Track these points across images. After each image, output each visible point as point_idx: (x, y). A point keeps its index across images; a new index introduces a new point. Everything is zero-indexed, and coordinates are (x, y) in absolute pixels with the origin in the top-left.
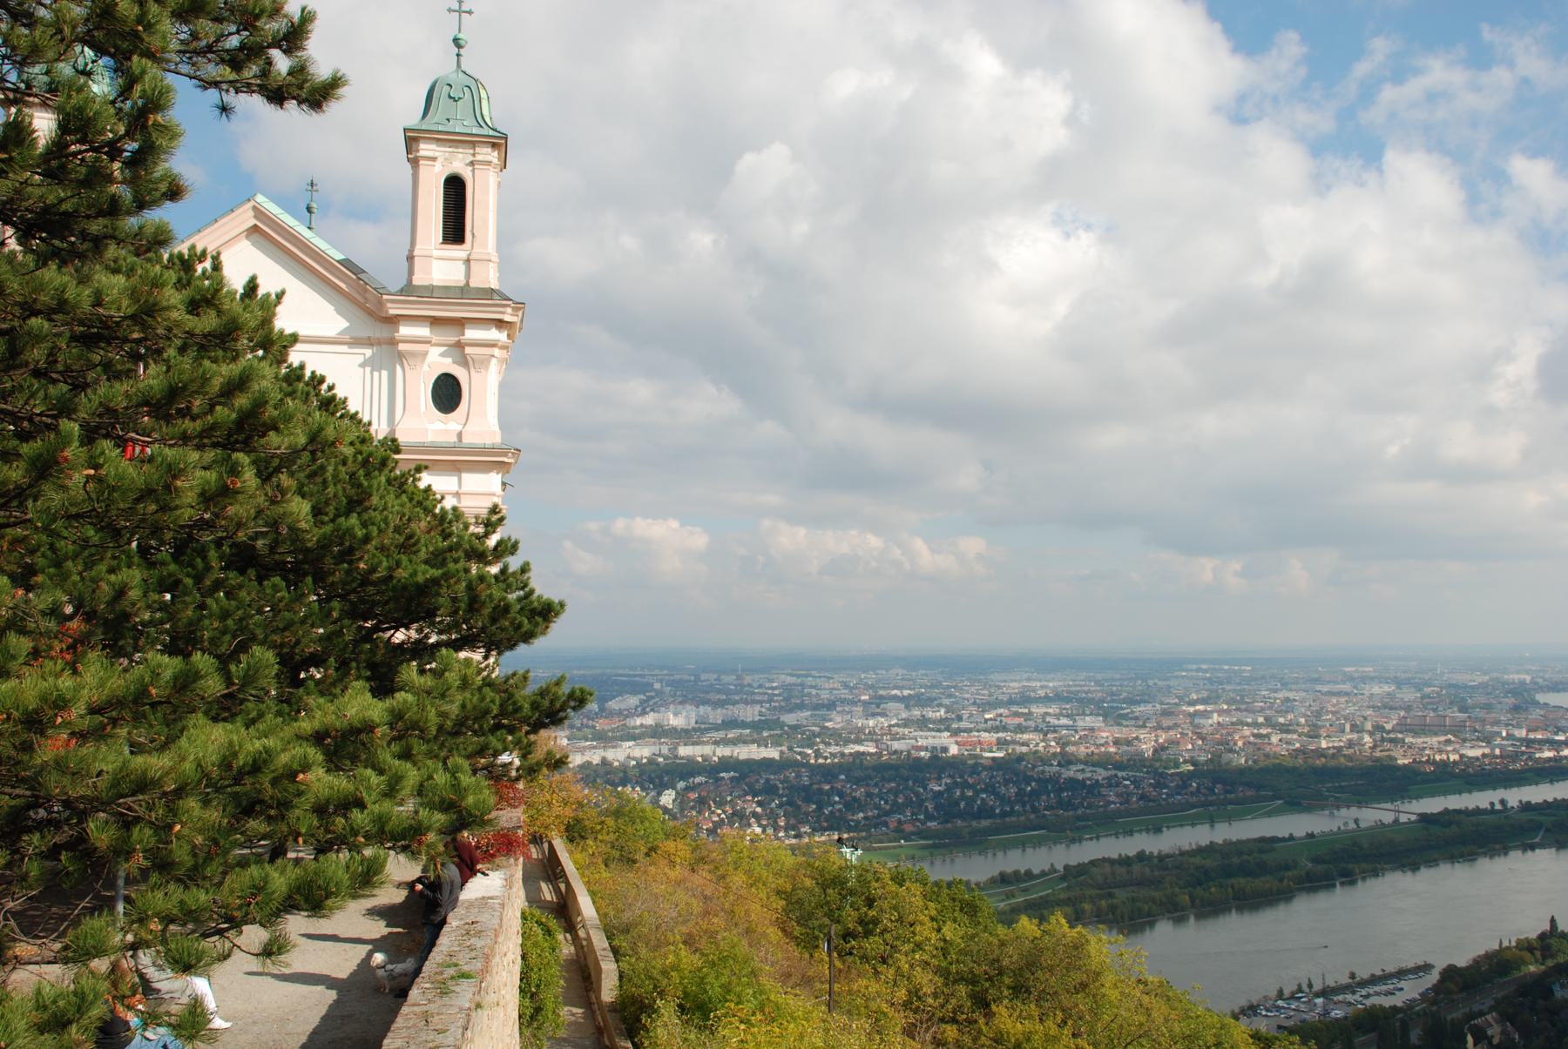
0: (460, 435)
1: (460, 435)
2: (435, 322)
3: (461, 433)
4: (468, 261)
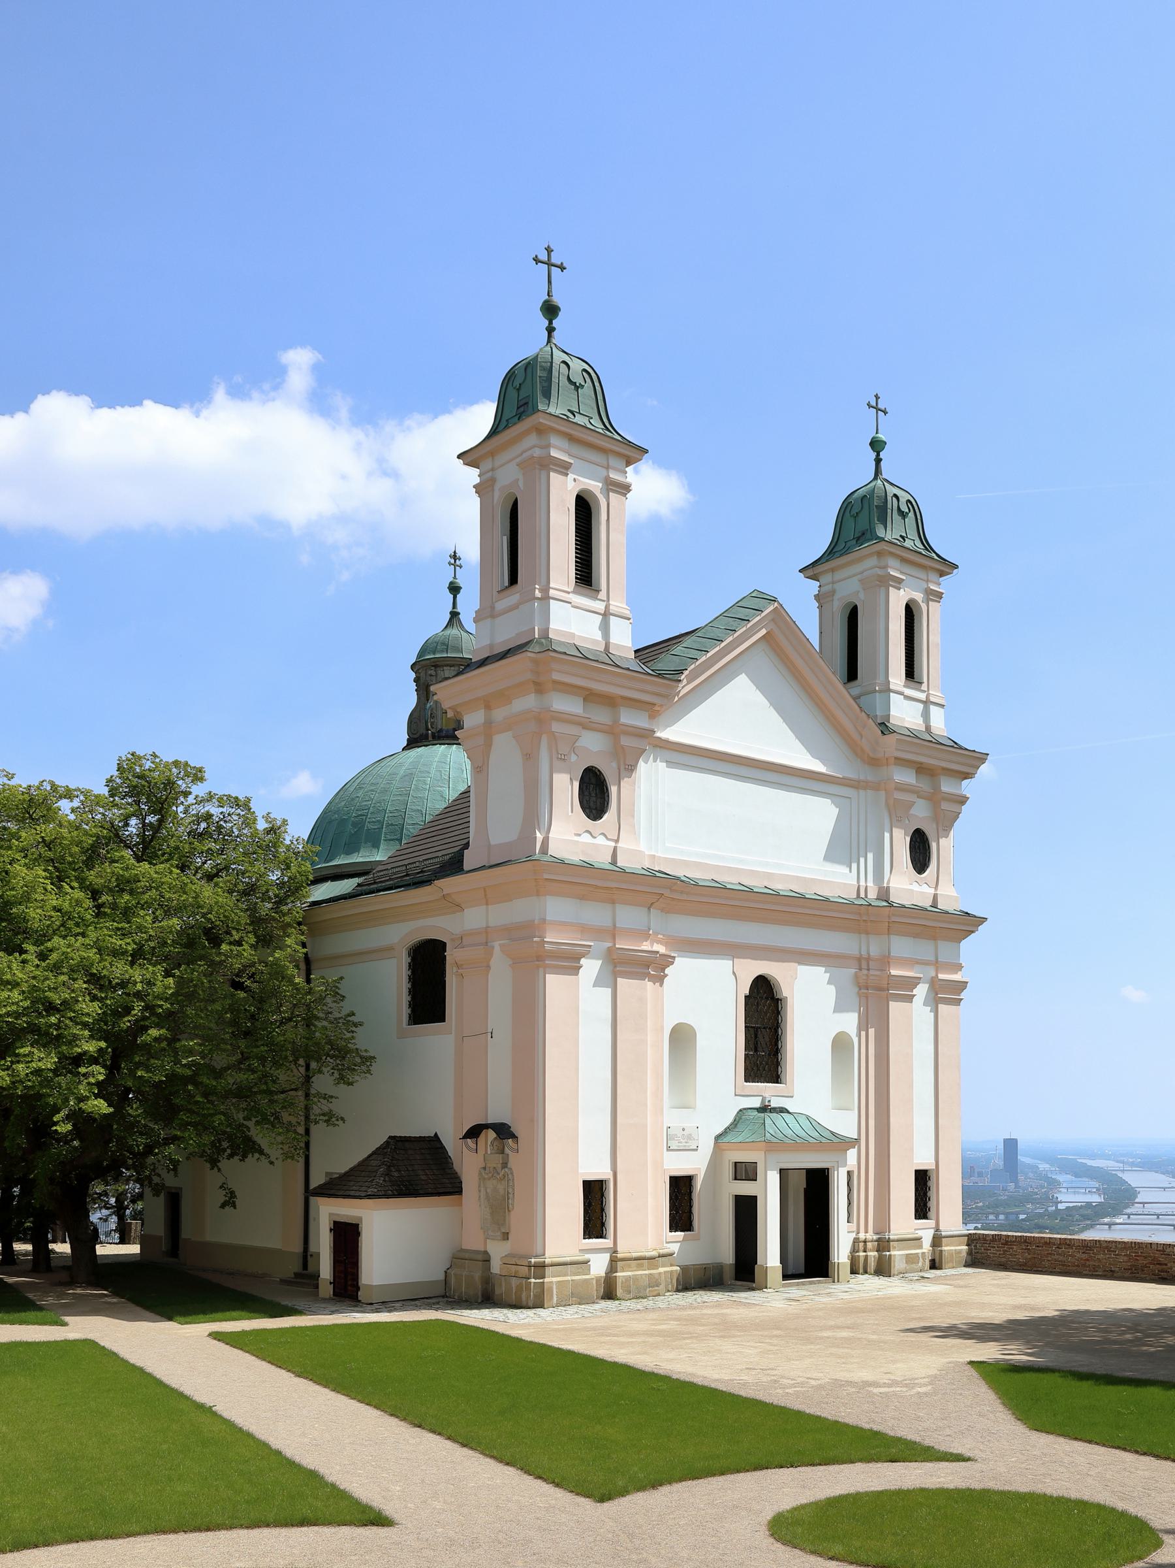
0: (935, 897)
1: (935, 897)
2: (590, 697)
3: (615, 849)
4: (606, 615)
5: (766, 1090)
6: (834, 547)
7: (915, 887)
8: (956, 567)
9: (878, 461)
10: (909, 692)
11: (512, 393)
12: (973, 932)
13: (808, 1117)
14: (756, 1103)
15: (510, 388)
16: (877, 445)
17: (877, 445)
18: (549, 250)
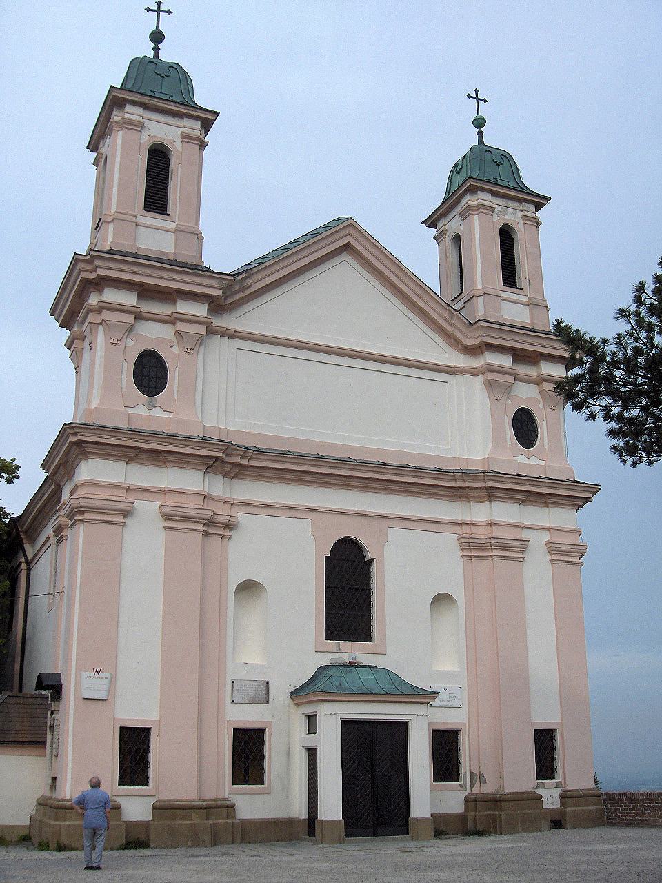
2: (145, 292)
5: (348, 650)
6: (450, 191)
7: (522, 459)
8: (549, 199)
9: (480, 134)
10: (504, 295)
11: (456, 177)
12: (588, 500)
13: (388, 672)
14: (346, 659)
15: (455, 173)
16: (479, 123)
17: (479, 123)
18: (477, 91)
